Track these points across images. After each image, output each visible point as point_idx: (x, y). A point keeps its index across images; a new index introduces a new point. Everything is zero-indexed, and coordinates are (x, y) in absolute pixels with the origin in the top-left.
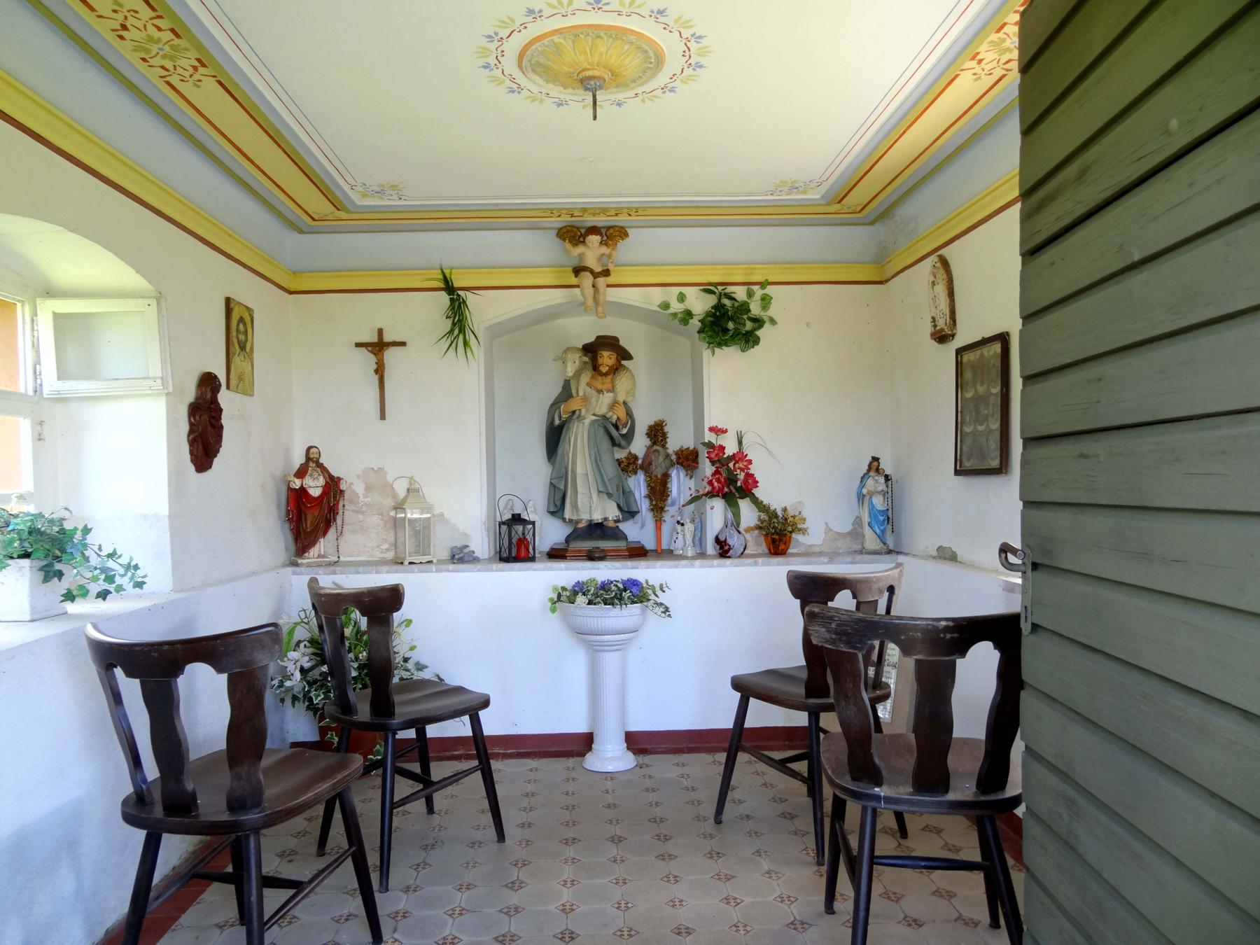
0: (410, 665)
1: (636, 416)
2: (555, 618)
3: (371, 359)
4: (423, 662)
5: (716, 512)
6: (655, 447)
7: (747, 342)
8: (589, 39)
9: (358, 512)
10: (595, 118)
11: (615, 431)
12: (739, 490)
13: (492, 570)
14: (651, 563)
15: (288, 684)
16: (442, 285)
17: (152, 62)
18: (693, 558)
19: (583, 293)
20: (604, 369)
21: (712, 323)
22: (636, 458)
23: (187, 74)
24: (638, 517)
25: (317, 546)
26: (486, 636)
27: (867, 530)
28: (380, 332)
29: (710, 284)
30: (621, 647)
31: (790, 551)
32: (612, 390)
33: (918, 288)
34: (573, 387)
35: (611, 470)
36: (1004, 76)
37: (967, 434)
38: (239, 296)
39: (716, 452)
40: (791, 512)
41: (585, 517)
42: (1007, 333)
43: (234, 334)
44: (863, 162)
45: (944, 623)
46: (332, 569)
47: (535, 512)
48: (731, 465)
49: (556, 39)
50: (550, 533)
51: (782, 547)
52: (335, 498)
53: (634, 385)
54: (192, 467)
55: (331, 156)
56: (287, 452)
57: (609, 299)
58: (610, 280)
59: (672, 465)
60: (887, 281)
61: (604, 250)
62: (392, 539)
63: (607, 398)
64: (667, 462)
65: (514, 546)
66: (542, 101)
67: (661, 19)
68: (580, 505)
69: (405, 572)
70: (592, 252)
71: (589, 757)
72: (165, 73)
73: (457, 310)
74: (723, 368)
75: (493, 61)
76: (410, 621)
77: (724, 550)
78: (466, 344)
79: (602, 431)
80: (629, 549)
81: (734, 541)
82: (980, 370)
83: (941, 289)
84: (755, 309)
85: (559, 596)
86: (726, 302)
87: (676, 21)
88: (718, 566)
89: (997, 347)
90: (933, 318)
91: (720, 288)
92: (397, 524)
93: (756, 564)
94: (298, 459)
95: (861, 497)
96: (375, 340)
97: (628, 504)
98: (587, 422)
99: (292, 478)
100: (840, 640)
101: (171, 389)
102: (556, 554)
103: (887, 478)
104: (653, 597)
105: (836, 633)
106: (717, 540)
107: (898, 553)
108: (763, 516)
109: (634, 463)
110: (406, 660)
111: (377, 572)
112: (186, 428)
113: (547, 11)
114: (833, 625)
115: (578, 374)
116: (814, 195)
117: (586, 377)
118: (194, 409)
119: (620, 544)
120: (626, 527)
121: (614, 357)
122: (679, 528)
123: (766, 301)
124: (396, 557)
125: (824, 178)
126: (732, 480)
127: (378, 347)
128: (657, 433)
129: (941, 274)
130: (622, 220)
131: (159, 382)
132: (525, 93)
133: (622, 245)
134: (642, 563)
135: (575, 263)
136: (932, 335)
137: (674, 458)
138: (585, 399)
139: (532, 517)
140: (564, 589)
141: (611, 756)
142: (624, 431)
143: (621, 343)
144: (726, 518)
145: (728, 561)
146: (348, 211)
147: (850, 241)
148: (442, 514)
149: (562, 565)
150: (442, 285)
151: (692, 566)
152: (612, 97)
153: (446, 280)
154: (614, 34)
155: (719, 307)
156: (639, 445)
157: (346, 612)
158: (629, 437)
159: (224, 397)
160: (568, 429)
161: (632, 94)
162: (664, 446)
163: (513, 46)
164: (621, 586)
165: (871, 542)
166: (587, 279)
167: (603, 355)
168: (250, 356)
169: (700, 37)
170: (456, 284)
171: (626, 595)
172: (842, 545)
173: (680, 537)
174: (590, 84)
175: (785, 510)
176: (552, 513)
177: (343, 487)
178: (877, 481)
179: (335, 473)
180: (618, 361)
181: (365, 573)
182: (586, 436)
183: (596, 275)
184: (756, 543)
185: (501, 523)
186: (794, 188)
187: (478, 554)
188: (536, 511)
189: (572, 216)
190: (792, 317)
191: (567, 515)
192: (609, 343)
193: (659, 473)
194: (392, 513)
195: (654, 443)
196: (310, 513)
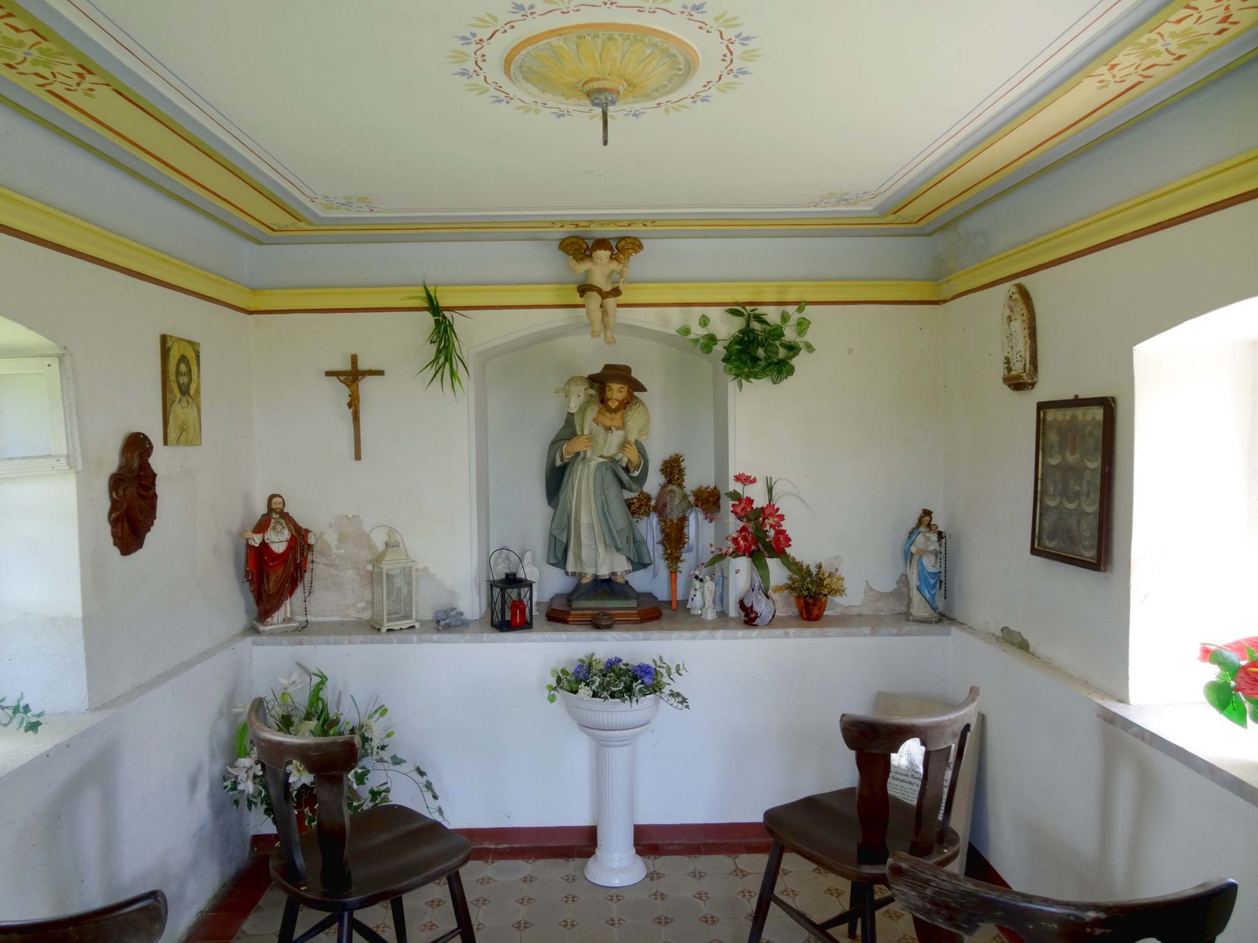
0: (386, 755)
3: (343, 392)
4: (400, 756)
5: (740, 571)
6: (671, 487)
7: (780, 373)
8: (599, 41)
10: (605, 143)
11: (624, 474)
13: (482, 641)
16: (425, 304)
17: (22, 68)
19: (588, 314)
20: (613, 405)
21: (739, 351)
22: (648, 498)
23: (73, 83)
25: (282, 609)
27: (915, 595)
28: (354, 359)
29: (737, 304)
32: (623, 427)
33: (986, 322)
34: (577, 423)
36: (1139, 83)
37: (1051, 508)
39: (744, 507)
40: (826, 569)
41: (590, 572)
42: (1113, 399)
43: (173, 378)
44: (931, 177)
45: (1092, 914)
49: (554, 41)
51: (816, 612)
52: (302, 554)
53: (648, 421)
54: (116, 551)
55: (280, 169)
58: (621, 299)
59: (690, 506)
60: (945, 301)
61: (615, 266)
63: (616, 437)
64: (684, 504)
65: (509, 609)
66: (537, 112)
67: (697, 16)
68: (584, 558)
69: (381, 642)
70: (600, 268)
72: (43, 81)
73: (443, 334)
74: (751, 400)
75: (471, 66)
77: (749, 618)
78: (453, 374)
79: (610, 476)
82: (1071, 435)
83: (1019, 327)
84: (790, 335)
85: (559, 680)
86: (756, 325)
87: (716, 19)
88: (743, 638)
89: (1098, 413)
90: (1008, 361)
91: (749, 308)
94: (261, 509)
95: (908, 556)
96: (348, 367)
99: (250, 535)
100: (938, 913)
101: (80, 467)
102: (558, 616)
105: (933, 903)
106: (742, 604)
111: (349, 643)
112: (106, 505)
113: (541, 7)
114: (929, 892)
115: (583, 409)
117: (592, 412)
118: (116, 482)
120: (640, 581)
122: (697, 584)
123: (803, 325)
126: (760, 535)
127: (352, 376)
128: (673, 469)
129: (1021, 308)
130: (635, 231)
131: (63, 461)
132: (515, 103)
133: (635, 258)
137: (692, 499)
138: (592, 438)
140: (564, 671)
141: (617, 865)
142: (636, 474)
143: (634, 375)
145: (754, 632)
146: (311, 224)
148: (426, 569)
150: (425, 304)
151: (714, 637)
152: (628, 107)
153: (430, 298)
154: (632, 35)
155: (747, 331)
156: (653, 483)
159: (158, 461)
161: (654, 103)
162: (680, 485)
163: (503, 43)
165: (920, 608)
166: (594, 300)
167: (613, 385)
169: (748, 38)
172: (886, 607)
173: (698, 594)
174: (600, 97)
175: (819, 566)
177: (311, 540)
178: (928, 539)
179: (304, 525)
181: (336, 643)
182: (591, 482)
183: (604, 295)
184: (783, 605)
185: (492, 585)
186: (844, 200)
191: (571, 567)
193: (675, 516)
195: (670, 482)
196: (273, 571)
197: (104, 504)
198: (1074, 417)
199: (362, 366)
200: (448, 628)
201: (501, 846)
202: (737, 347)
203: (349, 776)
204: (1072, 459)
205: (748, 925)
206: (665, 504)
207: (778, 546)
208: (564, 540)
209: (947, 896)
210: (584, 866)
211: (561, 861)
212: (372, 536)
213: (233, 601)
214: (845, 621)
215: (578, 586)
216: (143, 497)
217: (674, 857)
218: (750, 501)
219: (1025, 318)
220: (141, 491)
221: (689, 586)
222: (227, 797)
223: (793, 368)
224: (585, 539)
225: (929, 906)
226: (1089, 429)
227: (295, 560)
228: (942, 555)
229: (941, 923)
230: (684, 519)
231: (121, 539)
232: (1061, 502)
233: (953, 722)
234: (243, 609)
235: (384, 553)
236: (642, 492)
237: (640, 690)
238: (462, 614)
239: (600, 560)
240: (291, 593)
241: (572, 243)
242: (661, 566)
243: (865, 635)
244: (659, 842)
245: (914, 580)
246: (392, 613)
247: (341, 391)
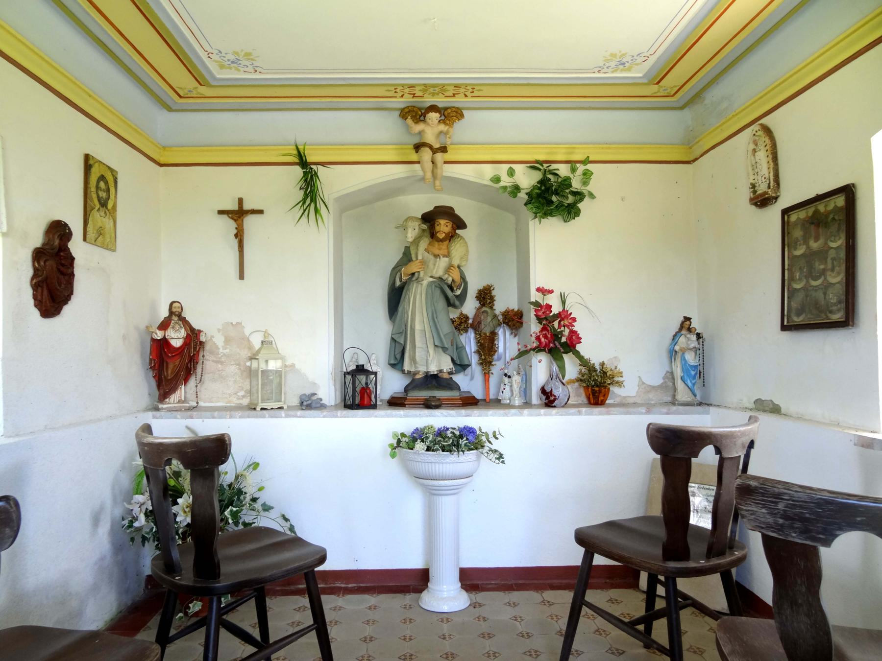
1: (468, 279)
2: (394, 465)
4: (269, 503)
5: (541, 368)
6: (484, 309)
7: (569, 213)
9: (217, 362)
11: (450, 292)
12: (565, 345)
13: (337, 417)
14: (483, 411)
15: (136, 524)
16: (297, 160)
18: (520, 407)
19: (423, 169)
20: (441, 236)
22: (467, 318)
24: (469, 370)
25: (178, 392)
26: (328, 480)
27: (680, 385)
28: (241, 201)
29: (537, 162)
31: (607, 402)
32: (448, 255)
35: (446, 328)
39: (544, 314)
40: (609, 366)
41: (422, 369)
46: (189, 413)
47: (377, 364)
48: (556, 324)
50: (390, 383)
51: (601, 398)
52: (195, 348)
53: (467, 251)
54: (36, 313)
56: (153, 307)
58: (448, 156)
59: (499, 325)
61: (442, 127)
62: (248, 387)
63: (443, 262)
65: (358, 394)
69: (257, 417)
70: (431, 129)
71: (425, 594)
74: (547, 236)
76: (258, 464)
77: (549, 400)
78: (316, 211)
79: (438, 292)
80: (462, 399)
81: (559, 391)
83: (763, 156)
84: (576, 185)
85: (399, 441)
88: (545, 415)
89: (840, 201)
91: (545, 165)
92: (251, 373)
93: (580, 413)
94: (164, 313)
95: (673, 354)
96: (236, 208)
98: (425, 283)
100: (792, 527)
102: (396, 402)
103: (699, 336)
104: (487, 444)
105: (785, 517)
106: (543, 391)
108: (584, 370)
109: (466, 322)
110: (254, 500)
111: (231, 417)
112: (30, 272)
114: (781, 506)
115: (416, 241)
116: (637, 73)
117: (424, 243)
118: (38, 255)
120: (458, 378)
121: (450, 225)
122: (506, 380)
123: (587, 175)
124: (251, 403)
125: (651, 52)
126: (556, 336)
128: (485, 296)
129: (764, 140)
130: (459, 101)
133: (458, 125)
134: (475, 412)
135: (416, 140)
136: (751, 200)
137: (501, 318)
138: (424, 263)
139: (374, 369)
140: (403, 435)
141: (446, 596)
142: (458, 292)
144: (551, 371)
147: (661, 126)
148: (293, 365)
149: (401, 412)
151: (521, 414)
153: (300, 155)
155: (543, 182)
156: (470, 307)
157: (169, 462)
158: (462, 298)
159: (77, 247)
160: (408, 289)
162: (491, 308)
164: (457, 433)
165: (683, 394)
166: (426, 154)
167: (441, 224)
168: (112, 213)
171: (463, 442)
173: (507, 388)
175: (602, 364)
176: (393, 366)
177: (203, 338)
178: (689, 339)
179: (196, 326)
180: (454, 229)
181: (220, 417)
182: (424, 296)
183: (435, 151)
184: (577, 395)
188: (378, 363)
189: (414, 96)
190: (609, 192)
191: (407, 366)
192: (446, 212)
193: (487, 331)
194: (248, 364)
195: (483, 305)
196: (173, 362)
197: (27, 271)
198: (816, 212)
199: (246, 207)
200: (309, 407)
201: (350, 586)
202: (537, 191)
204: (814, 245)
205: (559, 642)
207: (572, 343)
208: (402, 342)
209: (801, 507)
212: (251, 339)
213: (138, 381)
215: (413, 381)
216: (62, 273)
218: (549, 307)
219: (768, 147)
220: (61, 267)
221: (500, 382)
222: (127, 536)
223: (579, 210)
224: (419, 343)
225: (781, 521)
226: (831, 216)
228: (700, 352)
229: (795, 537)
230: (493, 335)
231: (41, 302)
233: (743, 434)
236: (462, 314)
237: (465, 445)
238: (321, 400)
239: (430, 359)
240: (186, 380)
241: (409, 112)
242: (476, 368)
243: (642, 413)
245: (678, 372)
246: (266, 394)
247: (228, 225)
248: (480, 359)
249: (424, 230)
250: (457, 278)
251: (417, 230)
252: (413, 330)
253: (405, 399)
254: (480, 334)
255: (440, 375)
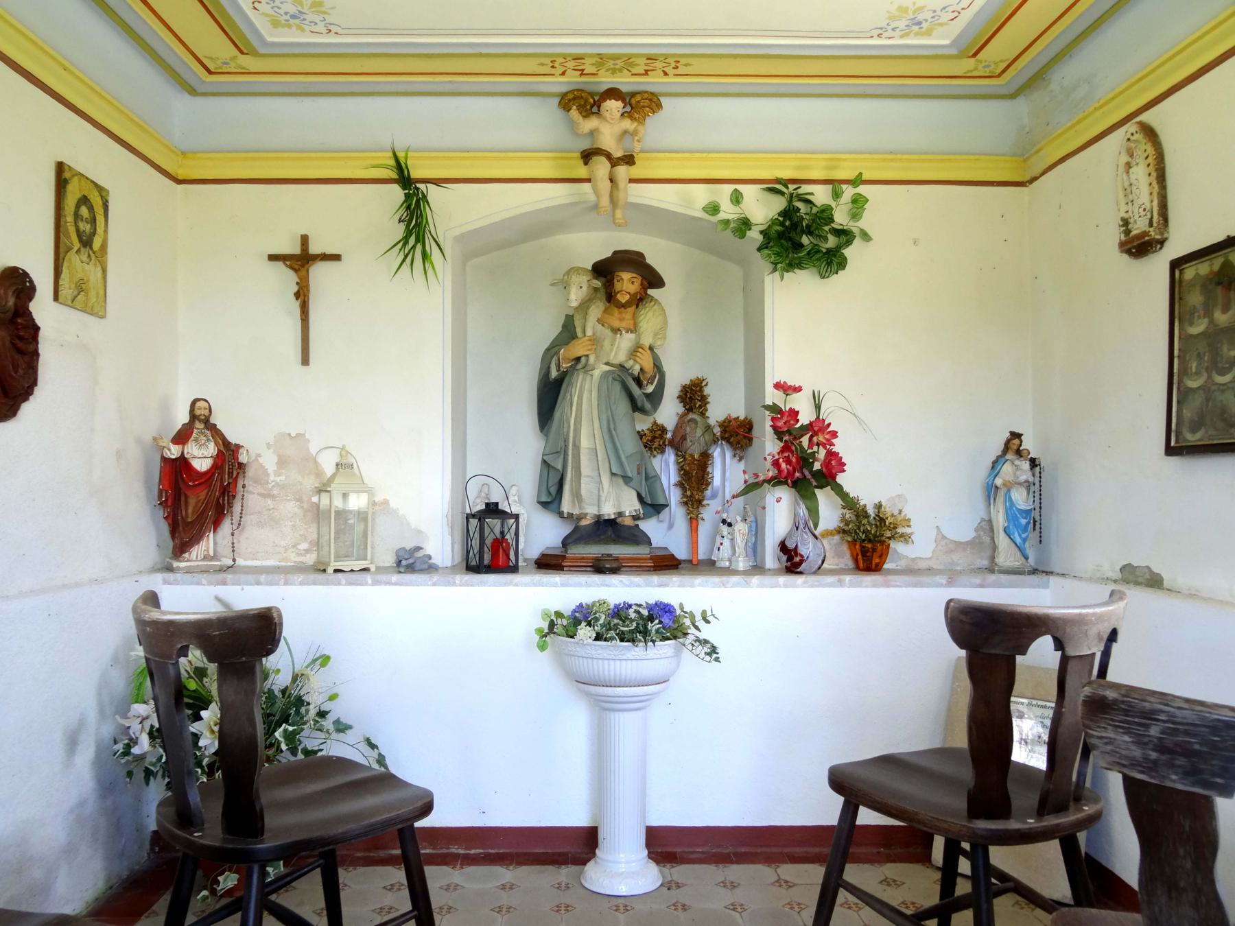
0: (328, 723)
1: (665, 368)
2: (543, 660)
5: (780, 509)
6: (691, 416)
7: (829, 264)
9: (265, 496)
11: (637, 389)
12: (818, 475)
13: (454, 584)
14: (687, 579)
16: (394, 175)
18: (745, 573)
19: (596, 191)
20: (623, 298)
21: (781, 235)
22: (663, 430)
25: (203, 543)
26: (439, 687)
27: (1002, 540)
28: (305, 240)
29: (778, 181)
30: (640, 704)
31: (886, 566)
32: (634, 329)
35: (630, 445)
38: (79, 162)
40: (888, 509)
41: (591, 511)
46: (221, 576)
47: (520, 502)
48: (805, 441)
50: (540, 532)
51: (876, 560)
52: (231, 474)
53: (665, 323)
56: (166, 406)
57: (631, 200)
58: (635, 171)
59: (715, 441)
60: (1033, 180)
61: (627, 124)
65: (489, 548)
68: (583, 493)
69: (327, 583)
70: (610, 128)
74: (792, 299)
76: (328, 658)
77: (792, 562)
78: (425, 256)
79: (617, 387)
81: (808, 548)
83: (1141, 175)
84: (841, 218)
85: (552, 625)
88: (786, 586)
90: (1126, 222)
91: (792, 187)
92: (319, 515)
93: (841, 583)
94: (182, 417)
95: (991, 491)
96: (297, 250)
97: (652, 493)
98: (597, 373)
102: (548, 563)
103: (1034, 463)
104: (692, 630)
105: (1161, 748)
106: (783, 547)
107: (1047, 573)
108: (849, 515)
109: (661, 437)
110: (322, 714)
111: (286, 583)
114: (1154, 731)
115: (584, 306)
116: (942, 39)
117: (596, 310)
119: (642, 551)
120: (649, 527)
121: (638, 281)
122: (725, 529)
123: (858, 203)
124: (318, 562)
126: (805, 460)
127: (301, 260)
128: (693, 396)
130: (654, 82)
134: (674, 579)
135: (586, 145)
137: (717, 430)
138: (595, 341)
139: (515, 509)
140: (559, 614)
141: (624, 870)
142: (650, 389)
143: (649, 260)
144: (795, 515)
145: (800, 580)
147: (981, 125)
149: (556, 578)
151: (748, 584)
153: (400, 167)
155: (788, 213)
156: (668, 413)
158: (656, 398)
160: (570, 383)
162: (703, 414)
164: (645, 613)
165: (1007, 555)
166: (601, 167)
167: (622, 278)
170: (415, 174)
171: (653, 627)
173: (726, 542)
175: (879, 506)
176: (545, 505)
177: (243, 458)
179: (233, 438)
180: (644, 288)
181: (269, 583)
182: (595, 393)
183: (614, 162)
184: (837, 554)
185: (469, 517)
187: (437, 560)
188: (521, 498)
190: (891, 226)
191: (566, 507)
193: (695, 451)
196: (195, 494)
199: (314, 249)
200: (411, 569)
201: (473, 852)
202: (778, 228)
203: (277, 734)
206: (687, 440)
207: (830, 471)
208: (559, 467)
209: (1187, 733)
210: (581, 872)
211: (550, 869)
212: (319, 460)
213: (142, 525)
214: (913, 572)
216: (20, 352)
217: (697, 867)
219: (1150, 160)
222: (120, 768)
223: (846, 259)
225: (1154, 755)
227: (222, 480)
228: (1035, 488)
229: (1175, 782)
230: (706, 457)
232: (1210, 377)
233: (1100, 618)
234: (154, 542)
235: (331, 480)
236: (655, 423)
237: (657, 631)
238: (430, 557)
239: (604, 495)
240: (216, 524)
241: (575, 99)
243: (941, 585)
244: (678, 850)
245: (1000, 520)
246: (341, 548)
247: (286, 278)
248: (684, 495)
249: (596, 289)
250: (648, 364)
251: (585, 289)
252: (577, 447)
253: (564, 557)
254: (684, 457)
255: (619, 520)
